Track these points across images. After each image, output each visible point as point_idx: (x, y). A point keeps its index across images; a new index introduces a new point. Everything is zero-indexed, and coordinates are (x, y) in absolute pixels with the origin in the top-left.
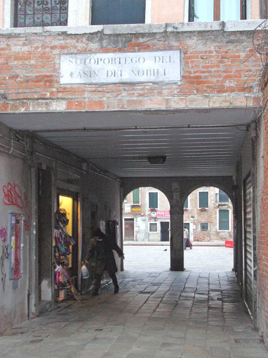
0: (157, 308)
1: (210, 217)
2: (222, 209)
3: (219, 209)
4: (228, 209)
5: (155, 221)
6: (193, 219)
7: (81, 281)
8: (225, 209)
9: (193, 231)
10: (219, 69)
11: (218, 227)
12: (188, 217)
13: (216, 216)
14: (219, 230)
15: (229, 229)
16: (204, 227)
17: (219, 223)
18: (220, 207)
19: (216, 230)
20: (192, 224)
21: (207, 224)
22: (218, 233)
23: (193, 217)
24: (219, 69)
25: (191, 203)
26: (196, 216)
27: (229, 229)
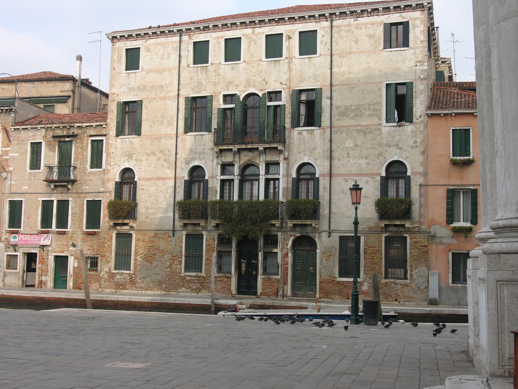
0: (354, 53)
1: (101, 245)
2: (122, 231)
3: (115, 232)
4: (132, 232)
5: (15, 251)
6: (74, 249)
7: (206, 214)
8: (126, 232)
9: (74, 270)
10: (199, 274)
11: (112, 264)
12: (67, 245)
13: (111, 245)
14: (115, 269)
15: (130, 270)
16: (94, 263)
17: (116, 255)
18: (118, 228)
19: (110, 269)
20: (72, 258)
21: (97, 258)
22: (112, 276)
23: (74, 245)
24: (199, 274)
25: (72, 220)
26: (79, 243)
27: (130, 270)
